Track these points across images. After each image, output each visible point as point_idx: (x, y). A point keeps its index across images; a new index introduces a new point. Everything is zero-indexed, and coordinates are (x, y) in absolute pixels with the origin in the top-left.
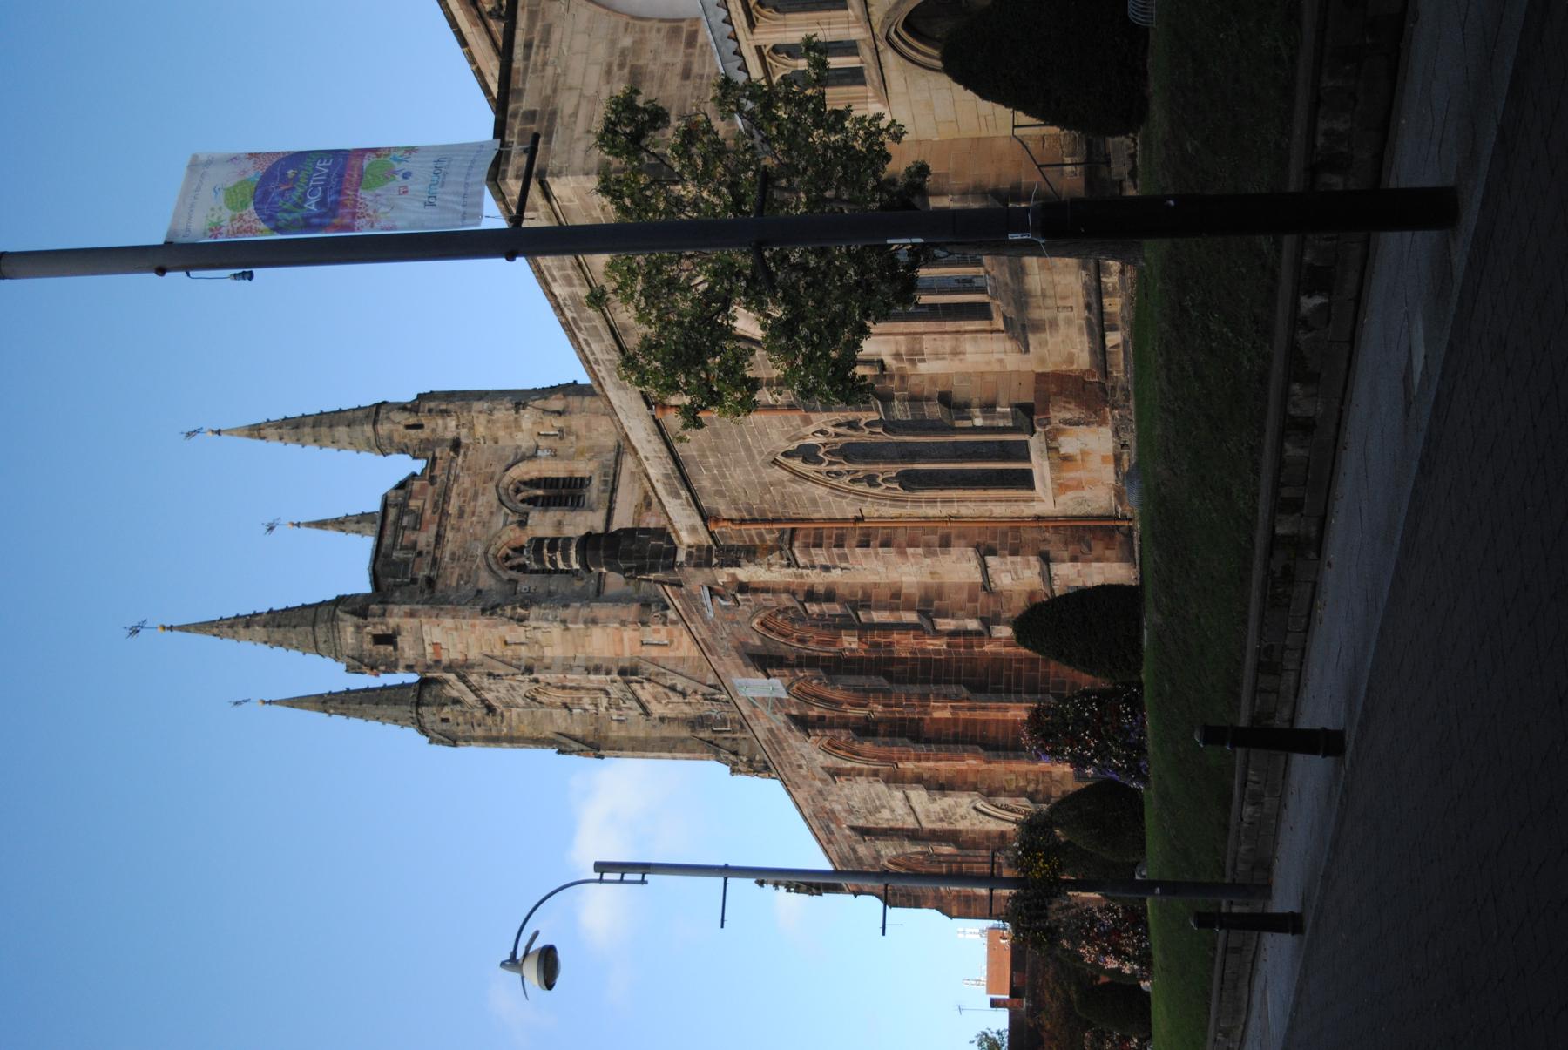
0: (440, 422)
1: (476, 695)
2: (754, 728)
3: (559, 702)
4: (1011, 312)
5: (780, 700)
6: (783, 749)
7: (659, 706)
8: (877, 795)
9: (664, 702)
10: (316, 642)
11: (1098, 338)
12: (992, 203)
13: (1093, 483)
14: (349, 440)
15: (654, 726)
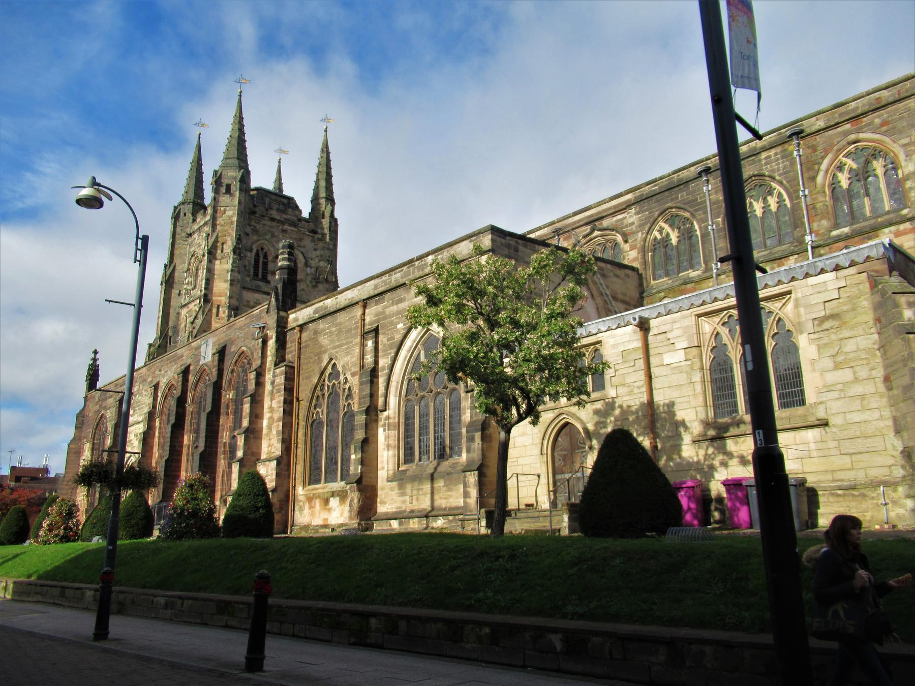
1: (197, 229)
2: (183, 348)
4: (409, 473)
5: (199, 360)
6: (171, 362)
7: (185, 313)
8: (141, 408)
10: (229, 158)
11: (395, 516)
13: (312, 514)
15: (175, 310)
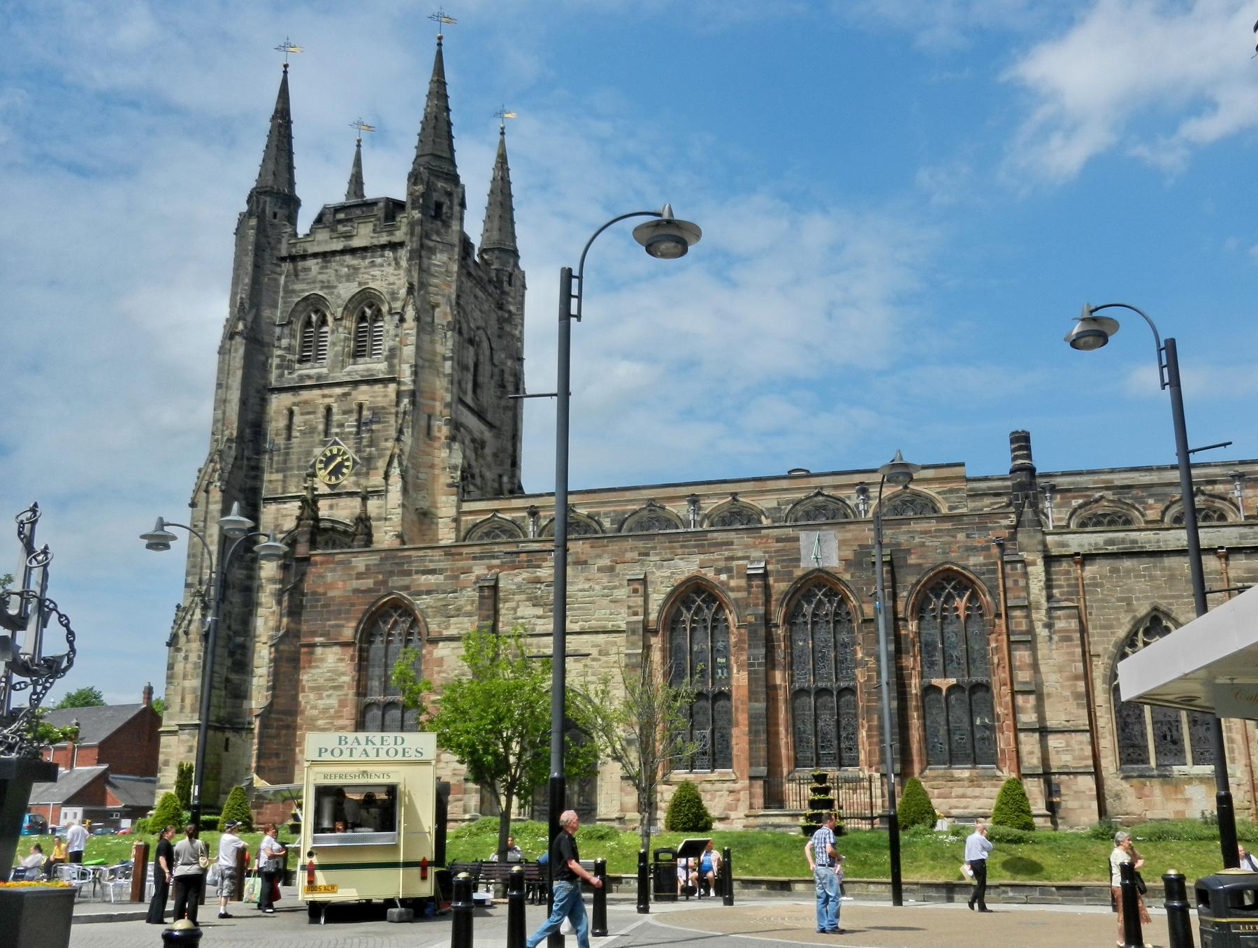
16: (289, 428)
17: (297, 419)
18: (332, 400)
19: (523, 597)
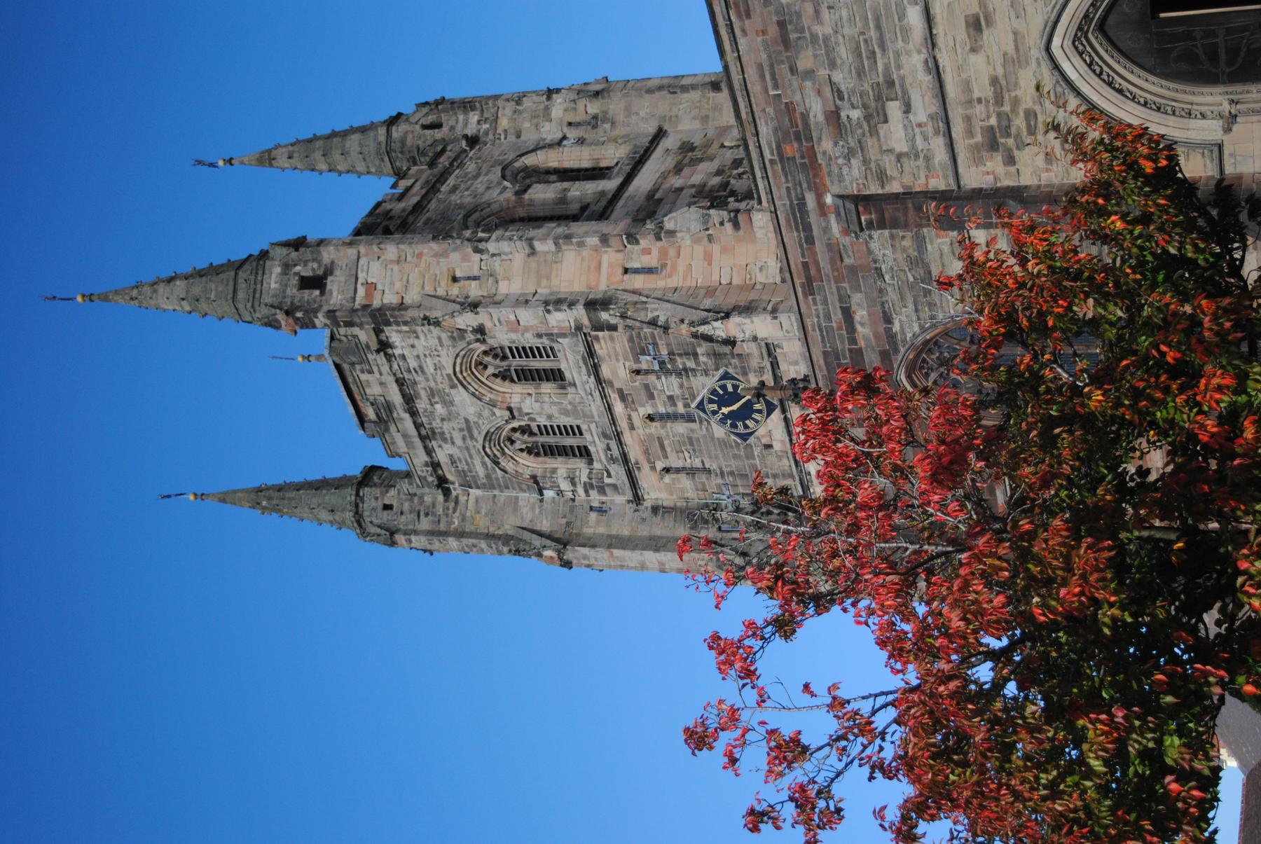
0: (461, 117)
3: (527, 473)
9: (660, 465)
12: (1174, 764)
14: (358, 149)
15: (644, 520)
16: (691, 472)
17: (675, 462)
18: (634, 415)
19: (870, 142)
